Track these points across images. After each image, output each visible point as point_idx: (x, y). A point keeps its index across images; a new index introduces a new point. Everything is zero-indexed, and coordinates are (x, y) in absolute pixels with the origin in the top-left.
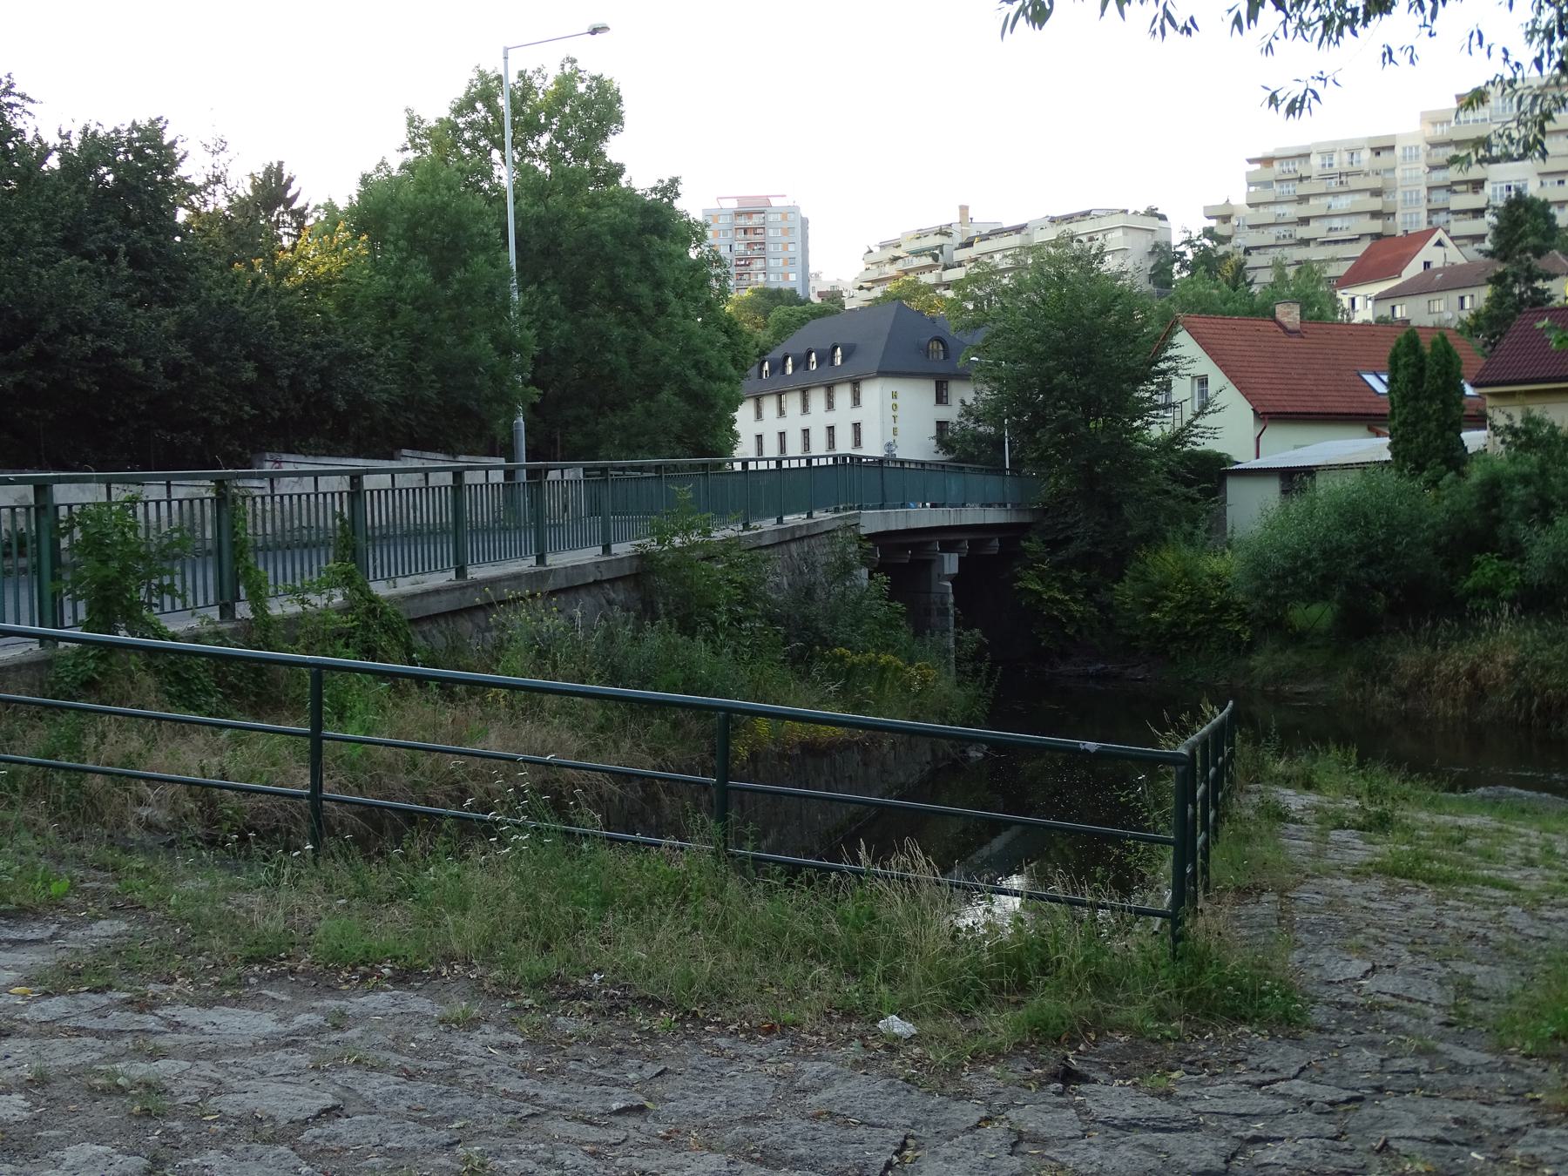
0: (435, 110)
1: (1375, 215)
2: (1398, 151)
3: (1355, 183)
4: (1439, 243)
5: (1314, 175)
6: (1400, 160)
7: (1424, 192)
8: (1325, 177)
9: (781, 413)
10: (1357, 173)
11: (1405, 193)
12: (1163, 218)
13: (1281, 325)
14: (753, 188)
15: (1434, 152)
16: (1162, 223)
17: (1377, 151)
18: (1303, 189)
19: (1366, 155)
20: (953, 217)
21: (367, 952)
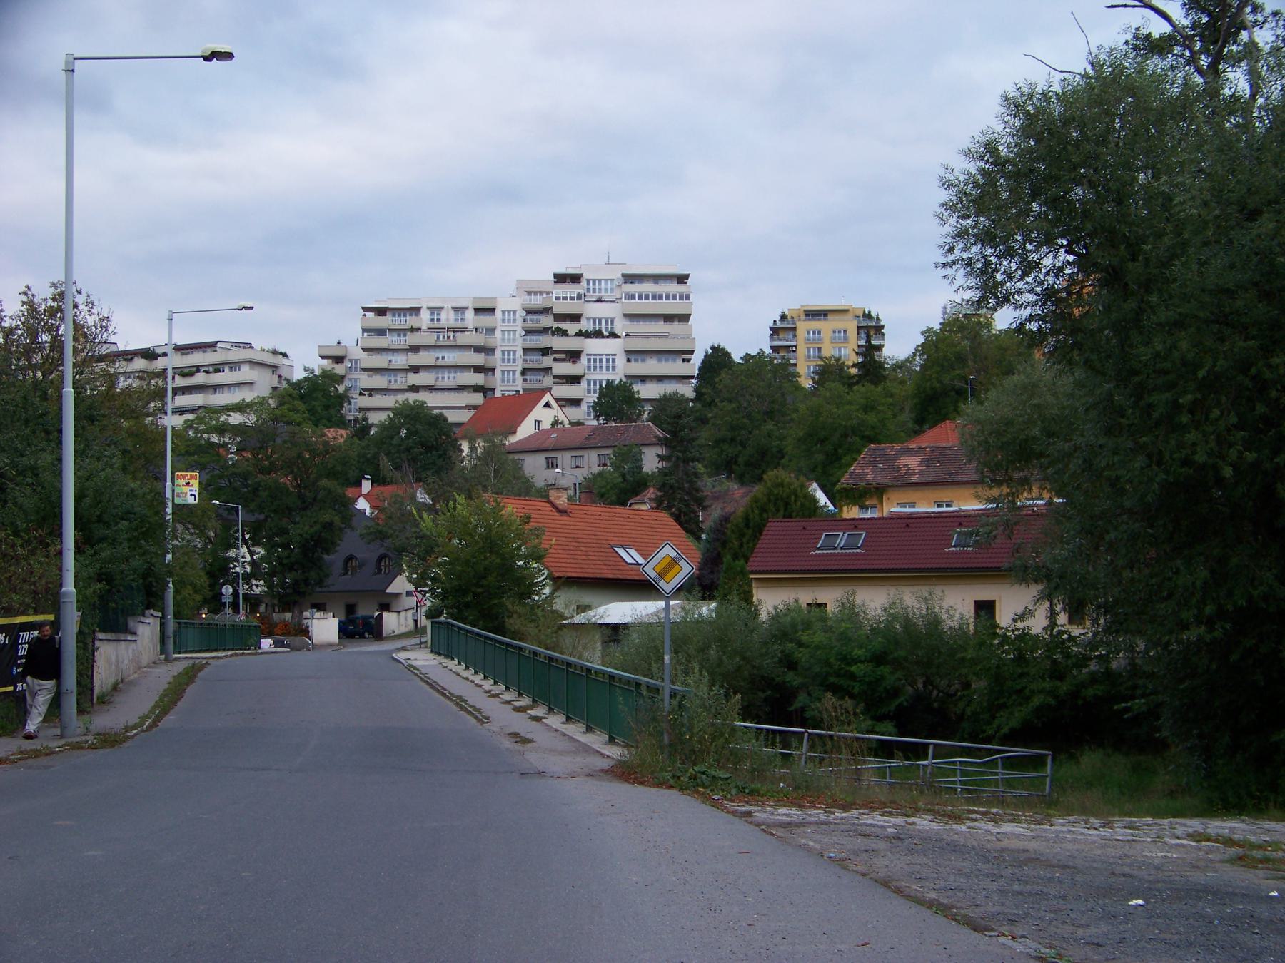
1: (478, 369)
2: (498, 313)
3: (462, 339)
4: (547, 405)
5: (424, 328)
6: (499, 322)
7: (520, 353)
8: (431, 330)
10: (463, 330)
11: (503, 352)
12: (285, 355)
13: (553, 505)
16: (285, 361)
17: (477, 311)
18: (413, 339)
19: (470, 315)
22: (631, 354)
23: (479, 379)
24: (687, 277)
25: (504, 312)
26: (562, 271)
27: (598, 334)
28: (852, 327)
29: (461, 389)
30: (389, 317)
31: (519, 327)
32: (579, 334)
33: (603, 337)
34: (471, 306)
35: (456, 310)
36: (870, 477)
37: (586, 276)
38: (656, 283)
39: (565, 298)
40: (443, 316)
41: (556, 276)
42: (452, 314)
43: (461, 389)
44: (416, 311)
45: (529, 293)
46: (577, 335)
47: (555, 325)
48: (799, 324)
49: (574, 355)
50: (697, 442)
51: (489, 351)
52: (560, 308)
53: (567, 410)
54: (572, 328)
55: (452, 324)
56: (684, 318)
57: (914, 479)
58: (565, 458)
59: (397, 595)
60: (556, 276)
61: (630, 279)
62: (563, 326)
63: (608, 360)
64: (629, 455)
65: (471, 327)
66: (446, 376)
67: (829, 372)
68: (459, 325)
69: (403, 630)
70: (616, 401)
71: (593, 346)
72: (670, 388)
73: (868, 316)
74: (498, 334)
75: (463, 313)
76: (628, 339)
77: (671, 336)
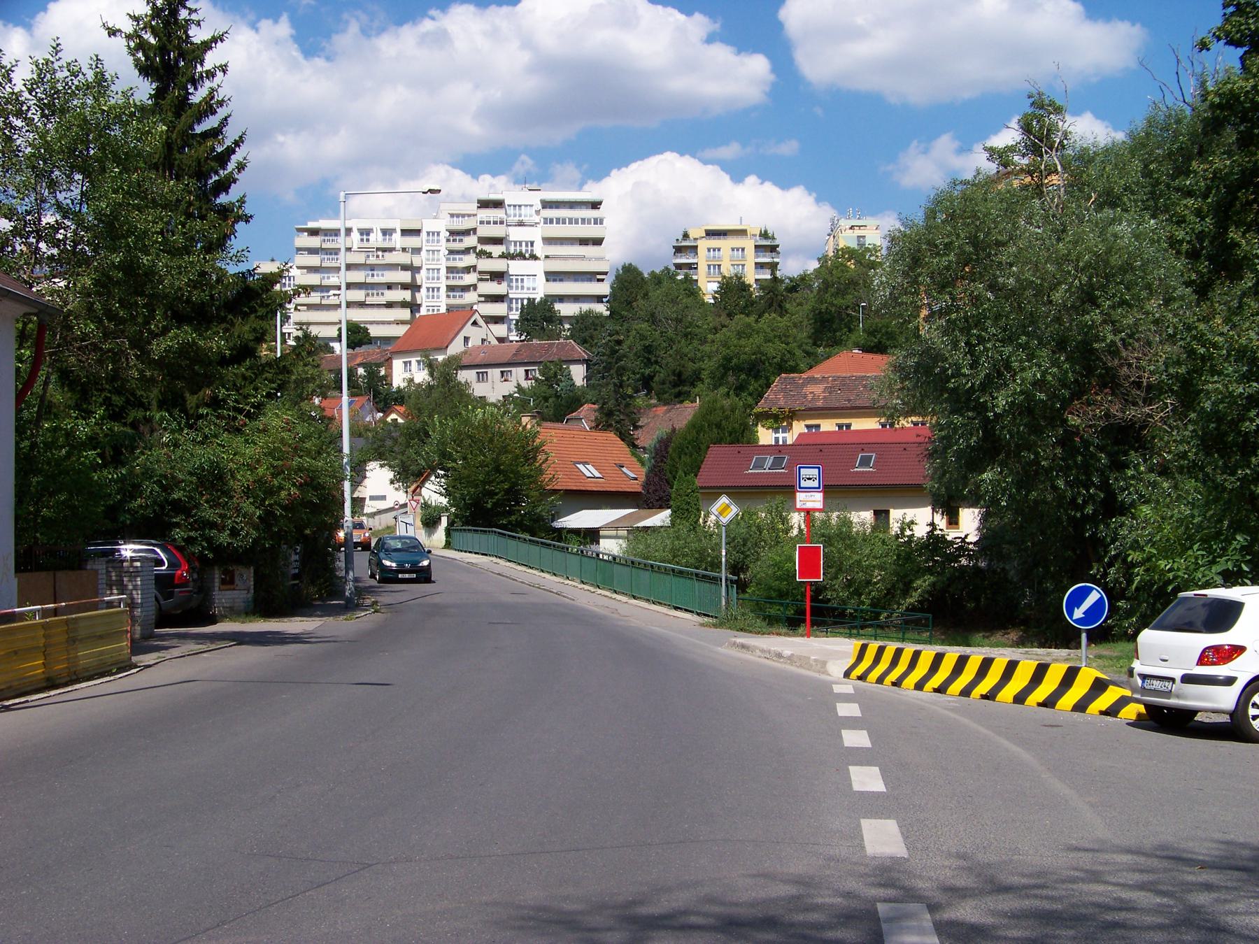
2: (424, 234)
4: (475, 323)
10: (391, 250)
17: (405, 232)
22: (552, 276)
23: (406, 295)
24: (600, 203)
25: (428, 233)
27: (521, 256)
28: (749, 244)
29: (390, 305)
31: (443, 247)
32: (503, 256)
33: (525, 258)
36: (782, 403)
37: (507, 203)
39: (489, 223)
41: (479, 201)
42: (380, 234)
43: (390, 305)
45: (452, 215)
46: (500, 257)
47: (479, 247)
48: (699, 243)
49: (498, 276)
50: (656, 379)
51: (413, 269)
52: (485, 231)
53: (491, 326)
54: (497, 250)
56: (598, 242)
57: (820, 404)
58: (495, 373)
60: (479, 201)
62: (488, 248)
64: (553, 374)
65: (398, 246)
67: (733, 288)
70: (538, 317)
71: (515, 267)
72: (586, 307)
73: (765, 235)
76: (548, 261)
77: (589, 258)
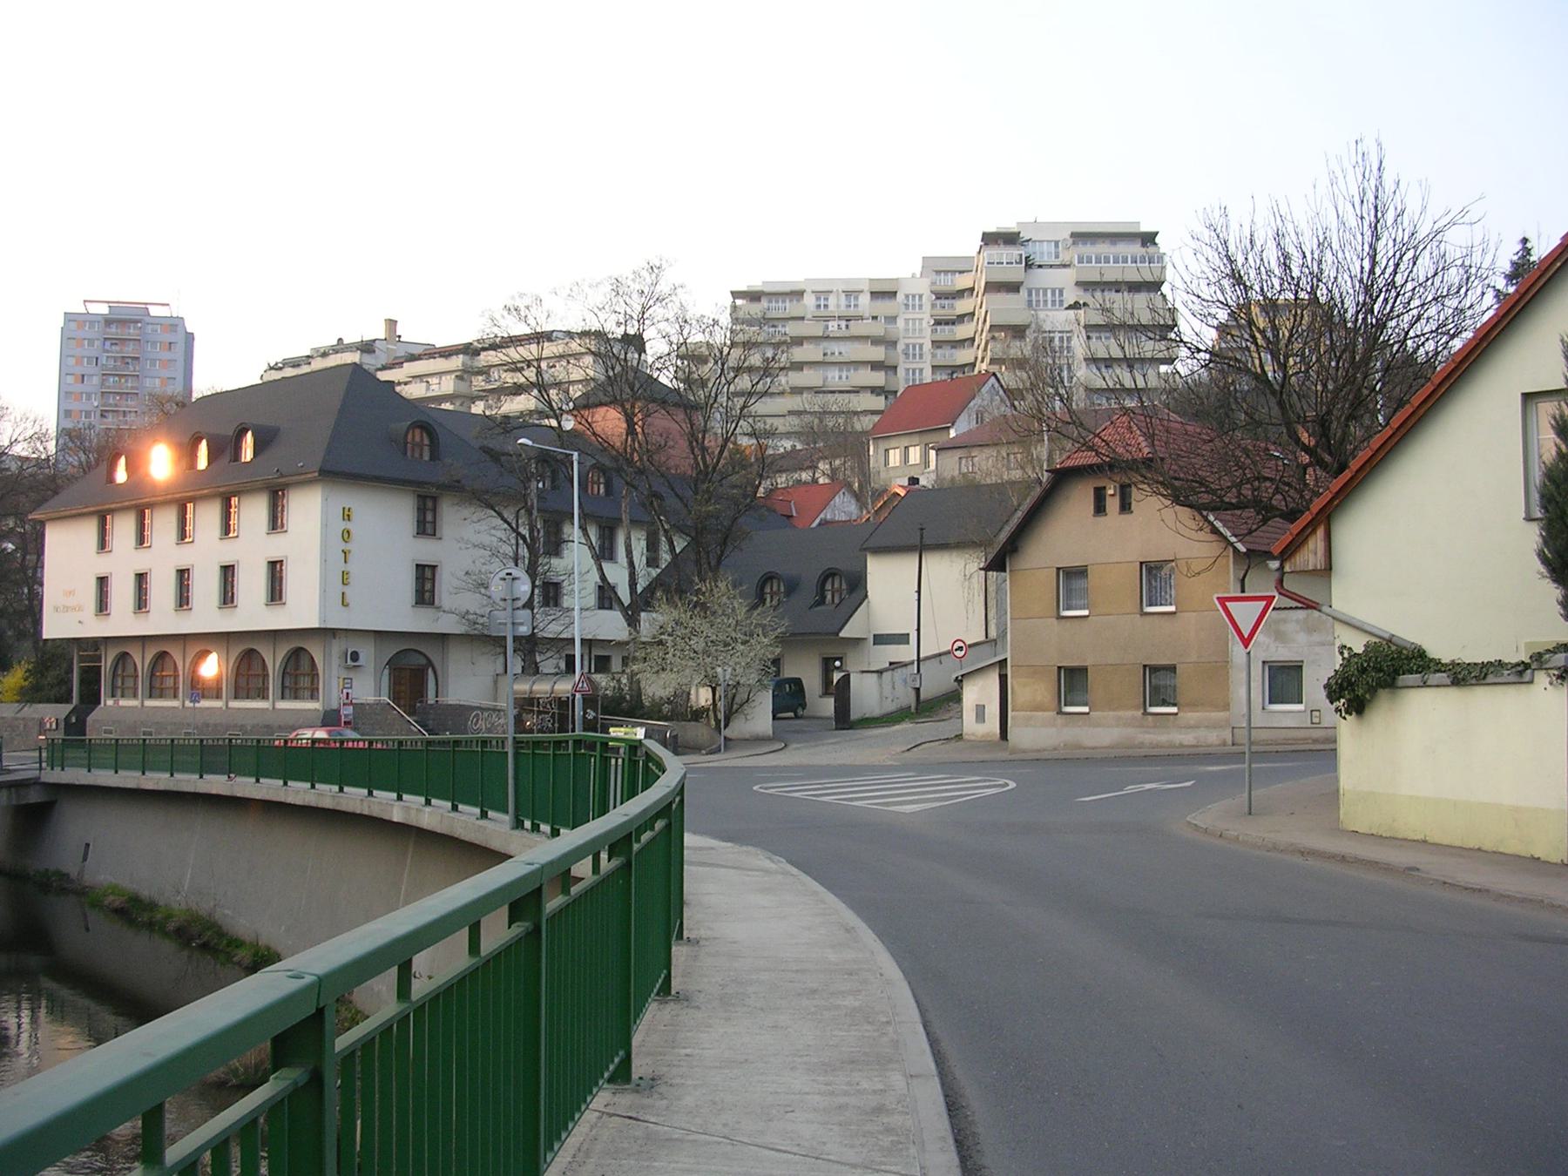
0: (413, 333)
1: (876, 366)
2: (900, 297)
3: (857, 328)
5: (809, 316)
7: (928, 346)
9: (141, 539)
14: (130, 292)
15: (939, 352)
17: (875, 295)
19: (865, 299)
20: (378, 332)
21: (1237, 279)
23: (878, 378)
25: (907, 296)
26: (992, 229)
30: (764, 303)
34: (866, 288)
35: (848, 294)
38: (1114, 243)
40: (832, 301)
44: (798, 294)
45: (938, 272)
55: (843, 311)
59: (857, 642)
61: (1080, 237)
63: (1061, 339)
66: (844, 375)
68: (852, 312)
69: (890, 707)
74: (900, 323)
75: (856, 298)
